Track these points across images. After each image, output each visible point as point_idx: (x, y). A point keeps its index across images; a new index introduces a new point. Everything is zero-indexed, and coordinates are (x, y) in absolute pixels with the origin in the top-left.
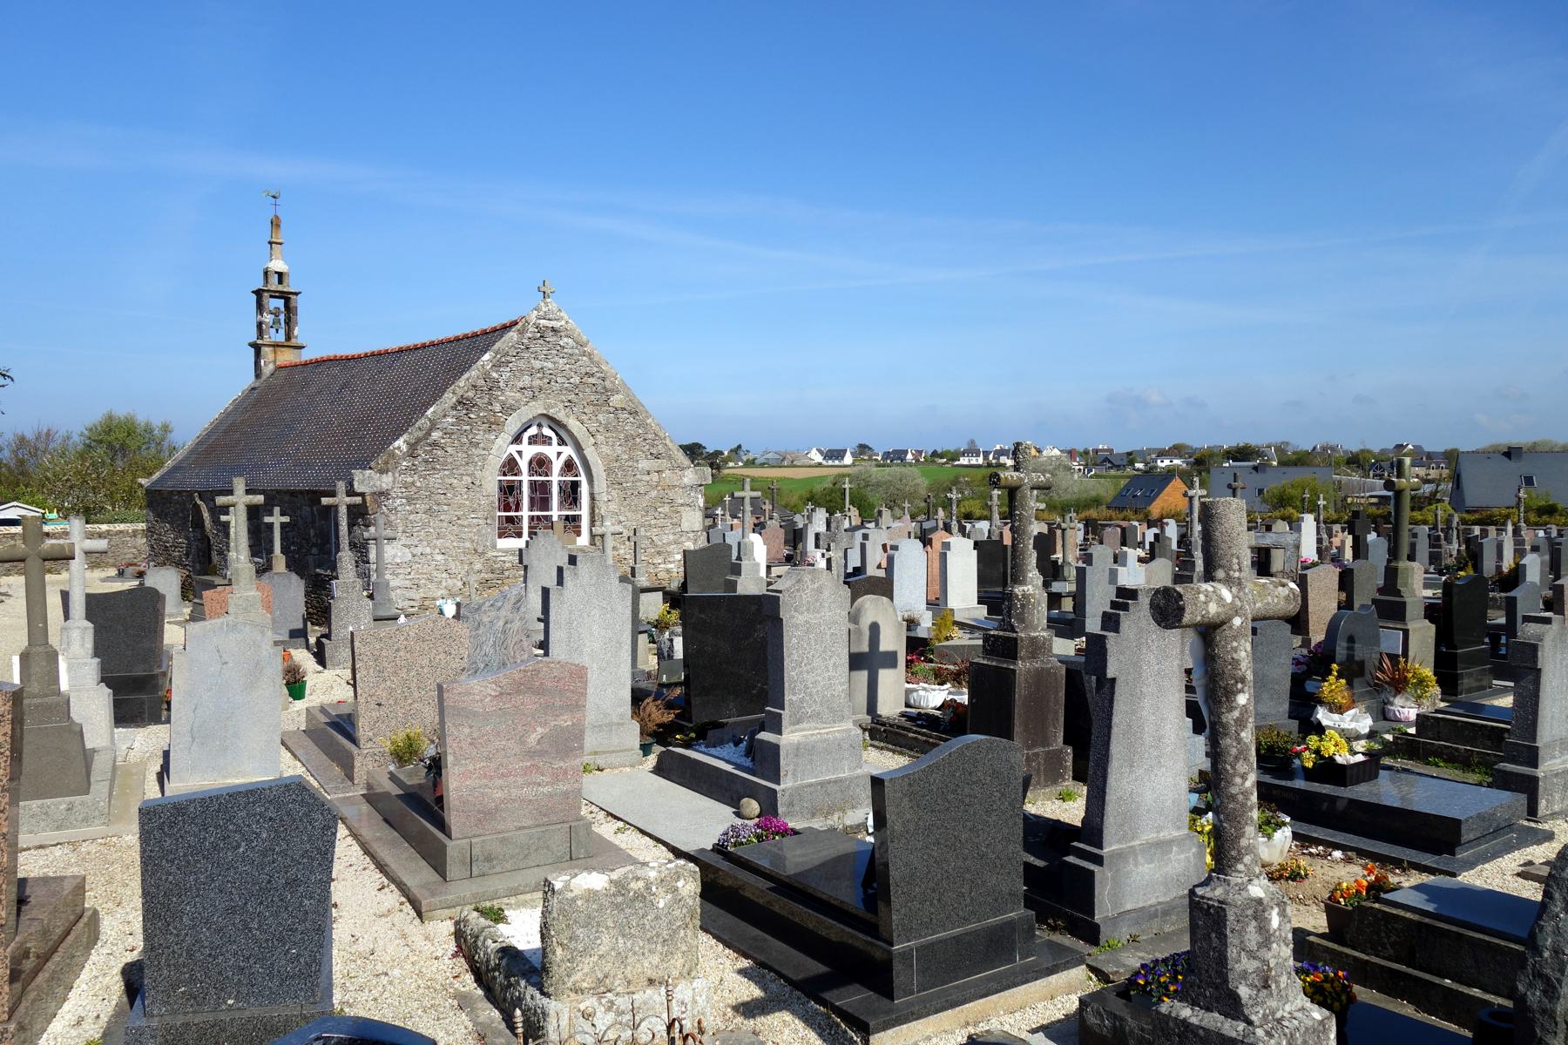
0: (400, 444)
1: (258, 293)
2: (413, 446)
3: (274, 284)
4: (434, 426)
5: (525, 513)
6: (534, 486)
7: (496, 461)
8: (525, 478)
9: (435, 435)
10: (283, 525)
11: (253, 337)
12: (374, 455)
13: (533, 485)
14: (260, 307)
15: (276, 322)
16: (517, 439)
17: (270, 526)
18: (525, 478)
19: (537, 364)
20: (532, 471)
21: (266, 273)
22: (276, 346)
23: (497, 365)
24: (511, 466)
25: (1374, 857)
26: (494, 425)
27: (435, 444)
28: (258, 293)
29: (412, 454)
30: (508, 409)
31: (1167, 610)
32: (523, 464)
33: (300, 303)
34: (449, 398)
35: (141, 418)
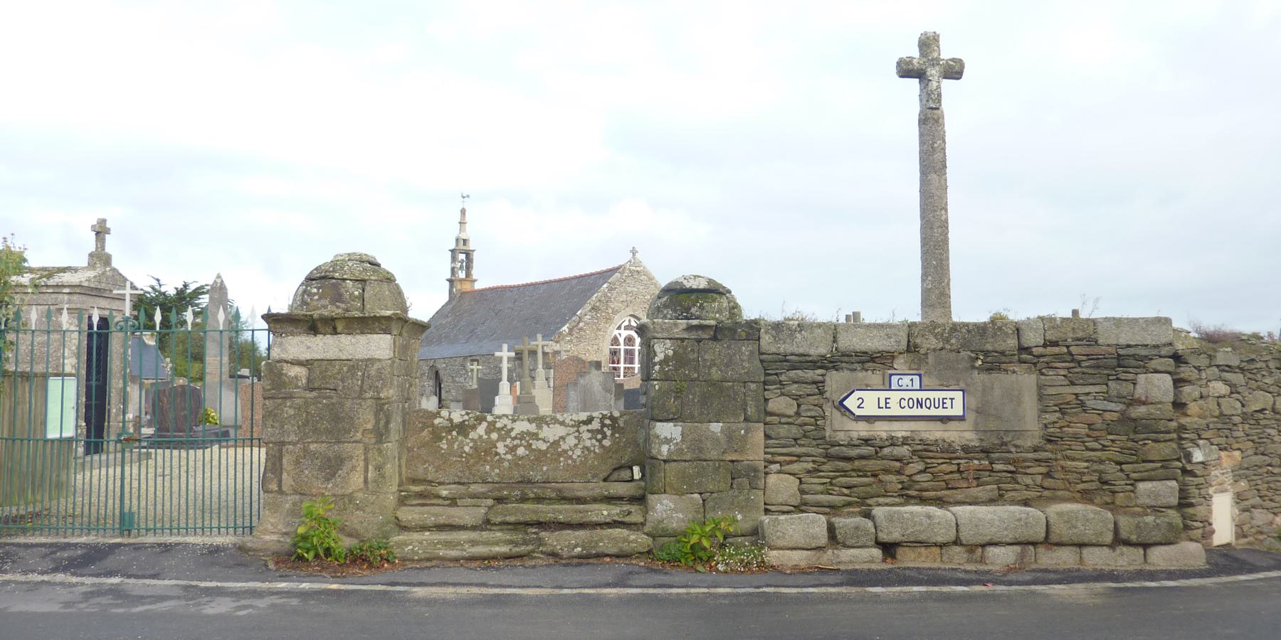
0: (565, 328)
1: (452, 251)
2: (571, 330)
3: (461, 247)
4: (580, 320)
5: (622, 365)
6: (626, 351)
7: (609, 339)
8: (622, 347)
9: (581, 324)
10: (509, 359)
11: (449, 276)
12: (553, 333)
13: (626, 351)
14: (454, 259)
15: (461, 267)
16: (619, 328)
17: (501, 359)
18: (622, 347)
19: (629, 289)
20: (625, 344)
21: (457, 240)
22: (461, 280)
23: (611, 289)
24: (615, 341)
25: (1152, 576)
26: (609, 320)
27: (581, 329)
28: (452, 251)
29: (571, 333)
30: (615, 312)
31: (540, 421)
32: (621, 340)
33: (475, 256)
34: (588, 307)
35: (1018, 313)
